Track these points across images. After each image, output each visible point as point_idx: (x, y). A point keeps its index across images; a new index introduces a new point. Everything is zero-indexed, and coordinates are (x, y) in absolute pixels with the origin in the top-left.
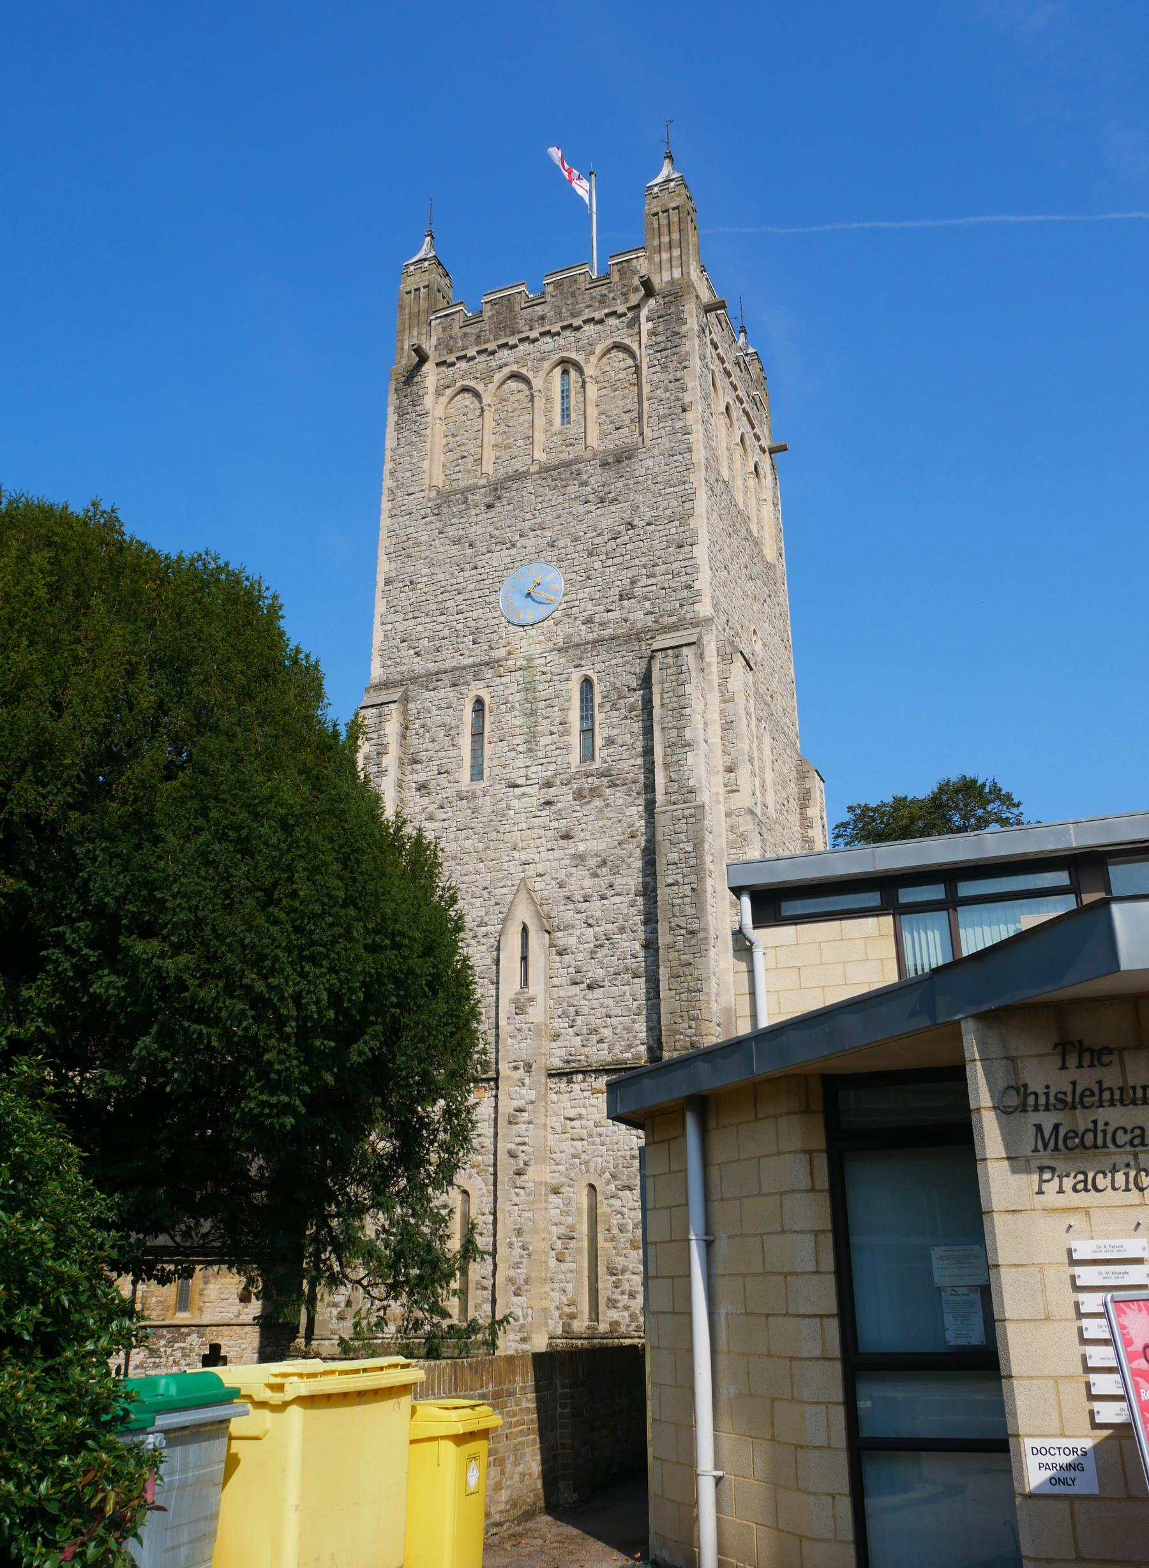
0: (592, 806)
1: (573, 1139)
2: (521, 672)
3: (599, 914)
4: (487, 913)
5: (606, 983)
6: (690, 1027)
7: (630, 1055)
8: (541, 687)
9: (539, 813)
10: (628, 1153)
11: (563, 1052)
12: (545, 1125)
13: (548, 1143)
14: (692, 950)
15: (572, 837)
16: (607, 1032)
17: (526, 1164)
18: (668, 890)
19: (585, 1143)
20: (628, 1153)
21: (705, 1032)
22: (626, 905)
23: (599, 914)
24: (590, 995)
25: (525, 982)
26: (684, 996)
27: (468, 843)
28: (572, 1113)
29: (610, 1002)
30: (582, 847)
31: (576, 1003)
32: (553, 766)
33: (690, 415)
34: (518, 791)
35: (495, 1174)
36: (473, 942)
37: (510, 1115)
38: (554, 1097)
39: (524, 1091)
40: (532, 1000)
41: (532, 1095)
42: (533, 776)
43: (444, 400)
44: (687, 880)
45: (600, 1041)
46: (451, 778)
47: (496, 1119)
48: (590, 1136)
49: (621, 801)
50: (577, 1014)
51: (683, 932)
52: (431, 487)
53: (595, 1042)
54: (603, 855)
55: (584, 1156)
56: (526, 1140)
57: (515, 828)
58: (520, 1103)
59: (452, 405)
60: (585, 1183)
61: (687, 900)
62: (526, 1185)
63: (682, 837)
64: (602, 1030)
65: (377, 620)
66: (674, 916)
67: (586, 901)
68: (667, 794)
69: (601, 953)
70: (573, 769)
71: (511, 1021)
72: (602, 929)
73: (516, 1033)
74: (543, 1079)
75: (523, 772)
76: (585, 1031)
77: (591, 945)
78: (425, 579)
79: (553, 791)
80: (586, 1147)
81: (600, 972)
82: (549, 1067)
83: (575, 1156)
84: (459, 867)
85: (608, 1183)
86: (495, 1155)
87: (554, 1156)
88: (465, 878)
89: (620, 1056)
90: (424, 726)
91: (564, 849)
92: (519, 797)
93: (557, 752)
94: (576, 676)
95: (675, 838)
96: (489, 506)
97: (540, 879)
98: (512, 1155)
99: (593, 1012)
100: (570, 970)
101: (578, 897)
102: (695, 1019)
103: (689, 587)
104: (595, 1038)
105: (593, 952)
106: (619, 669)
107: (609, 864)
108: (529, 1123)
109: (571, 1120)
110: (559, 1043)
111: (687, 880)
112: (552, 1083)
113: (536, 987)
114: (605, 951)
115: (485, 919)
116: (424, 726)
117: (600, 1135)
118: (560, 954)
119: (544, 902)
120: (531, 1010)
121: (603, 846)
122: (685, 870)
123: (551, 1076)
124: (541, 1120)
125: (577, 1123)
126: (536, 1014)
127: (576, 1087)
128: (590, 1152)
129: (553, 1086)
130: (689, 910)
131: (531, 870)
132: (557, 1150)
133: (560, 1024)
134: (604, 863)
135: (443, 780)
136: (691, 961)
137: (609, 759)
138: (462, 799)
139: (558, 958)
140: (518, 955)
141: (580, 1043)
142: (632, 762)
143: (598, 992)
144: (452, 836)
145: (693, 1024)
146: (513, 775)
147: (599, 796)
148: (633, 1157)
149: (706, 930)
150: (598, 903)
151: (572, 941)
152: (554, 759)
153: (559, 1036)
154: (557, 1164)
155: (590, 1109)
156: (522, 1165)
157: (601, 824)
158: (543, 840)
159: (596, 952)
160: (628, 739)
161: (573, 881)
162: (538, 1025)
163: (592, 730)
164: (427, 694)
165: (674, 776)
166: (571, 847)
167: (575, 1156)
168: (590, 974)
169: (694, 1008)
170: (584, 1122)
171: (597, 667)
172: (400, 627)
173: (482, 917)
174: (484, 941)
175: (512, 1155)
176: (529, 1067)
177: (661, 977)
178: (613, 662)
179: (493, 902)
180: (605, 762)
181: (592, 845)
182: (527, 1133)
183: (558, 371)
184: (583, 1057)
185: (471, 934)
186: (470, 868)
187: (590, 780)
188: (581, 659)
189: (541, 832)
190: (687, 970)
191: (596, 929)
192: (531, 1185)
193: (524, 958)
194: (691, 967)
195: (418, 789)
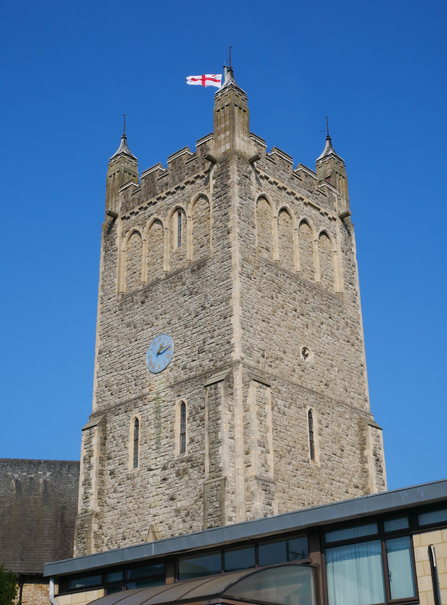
2: (154, 402)
15: (175, 499)
43: (125, 239)
52: (118, 293)
59: (129, 242)
183: (176, 214)
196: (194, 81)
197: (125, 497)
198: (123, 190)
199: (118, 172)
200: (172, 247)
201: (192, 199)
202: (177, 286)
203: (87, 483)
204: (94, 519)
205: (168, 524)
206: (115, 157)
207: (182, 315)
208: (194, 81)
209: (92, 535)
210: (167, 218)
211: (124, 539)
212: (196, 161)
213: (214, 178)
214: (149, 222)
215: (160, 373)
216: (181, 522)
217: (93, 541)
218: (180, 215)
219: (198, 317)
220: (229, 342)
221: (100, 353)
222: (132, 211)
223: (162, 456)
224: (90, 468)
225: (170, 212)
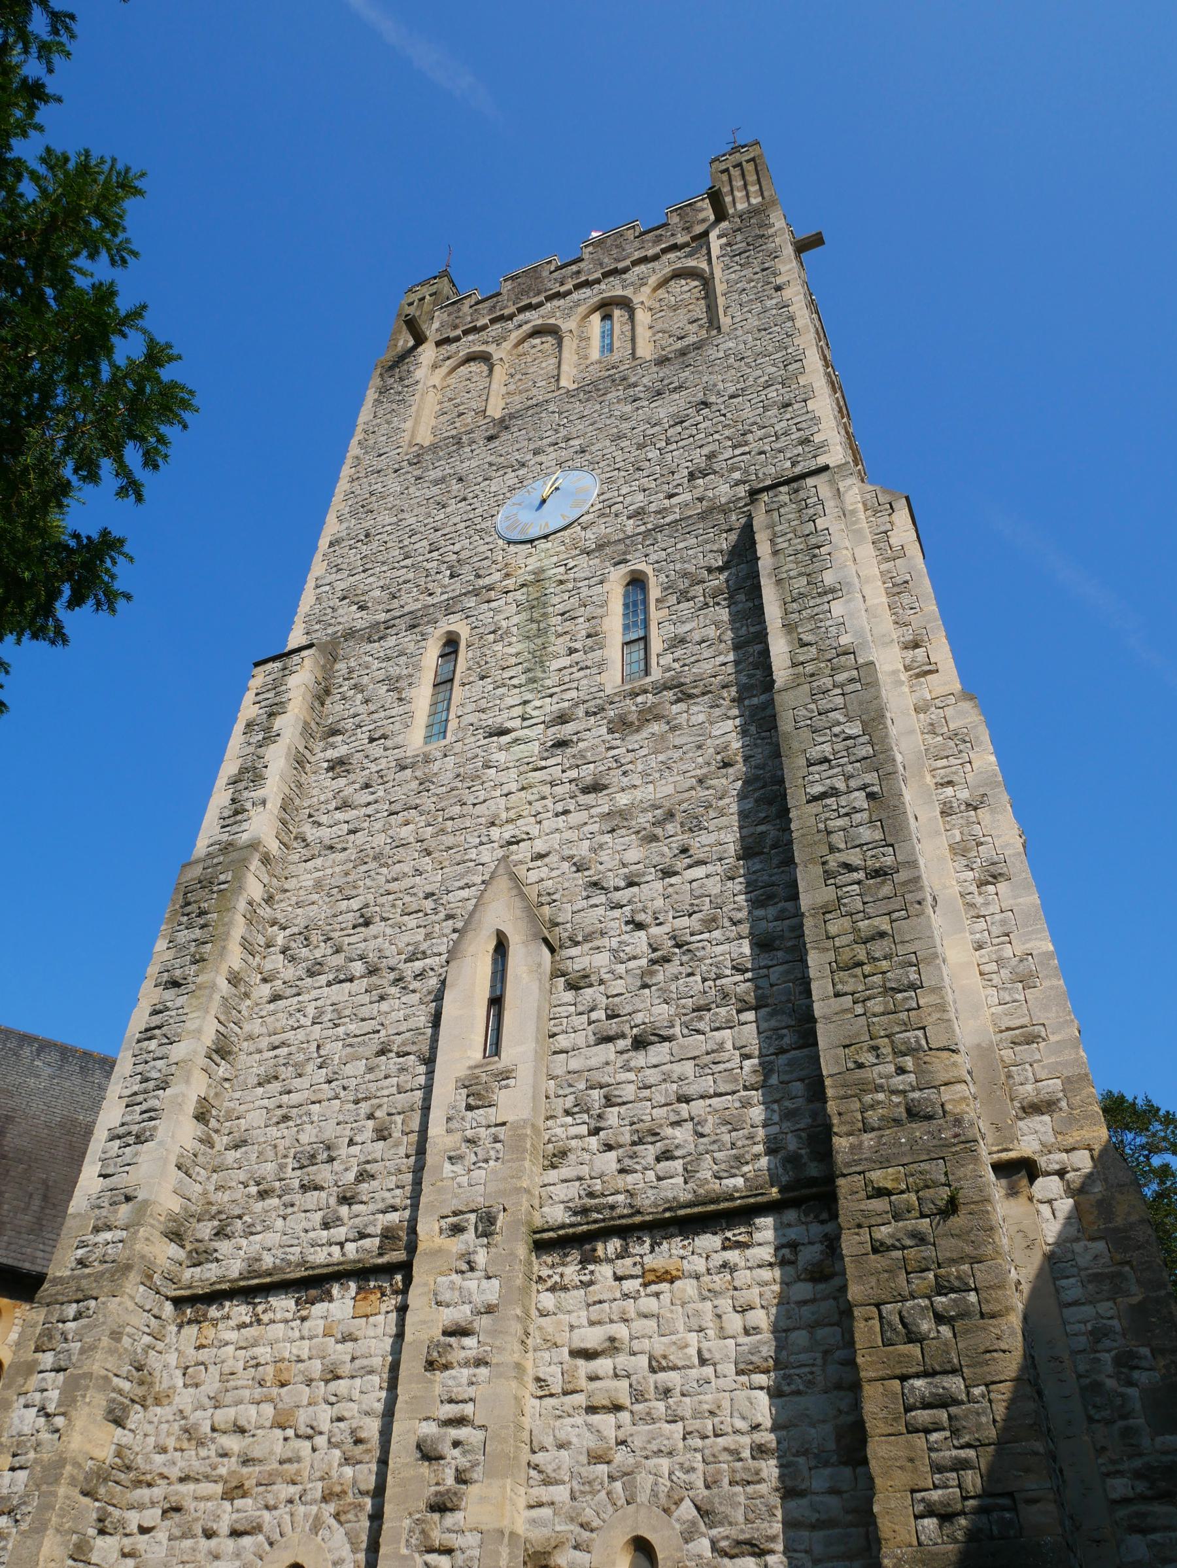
0: (645, 734)
1: (592, 1410)
2: (524, 590)
3: (659, 903)
4: (428, 936)
5: (677, 1030)
6: (901, 1071)
7: (739, 1182)
8: (556, 600)
9: (543, 763)
10: (746, 1440)
11: (573, 1191)
12: (519, 1366)
13: (526, 1422)
14: (884, 907)
15: (606, 787)
16: (682, 1135)
17: (461, 1478)
18: (815, 808)
19: (625, 1416)
20: (746, 1440)
21: (944, 1076)
22: (716, 877)
23: (659, 903)
24: (639, 1059)
25: (494, 1045)
26: (876, 1005)
27: (406, 832)
28: (592, 1338)
29: (688, 1068)
30: (623, 800)
31: (606, 1079)
32: (574, 694)
33: (787, 293)
34: (505, 739)
35: (377, 1517)
36: (393, 990)
37: (433, 1345)
38: (548, 1300)
39: (471, 1284)
40: (505, 1076)
41: (491, 1291)
42: (535, 713)
43: (444, 370)
44: (853, 783)
45: (665, 1156)
46: (389, 743)
47: (394, 1368)
48: (638, 1396)
49: (701, 718)
50: (609, 1102)
51: (860, 875)
52: (411, 445)
53: (651, 1159)
54: (667, 804)
55: (621, 1457)
56: (468, 1409)
57: (498, 793)
58: (460, 1314)
59: (453, 375)
60: (620, 1537)
61: (857, 817)
62: (456, 1541)
63: (837, 716)
64: (669, 1131)
65: (310, 583)
66: (832, 849)
67: (631, 884)
68: (794, 665)
69: (661, 975)
70: (609, 691)
71: (454, 1125)
72: (666, 928)
73: (464, 1148)
74: (522, 1250)
75: (518, 711)
76: (626, 1138)
77: (644, 962)
78: (389, 528)
79: (569, 728)
80: (628, 1428)
81: (663, 1011)
82: (538, 1222)
83: (596, 1458)
84: (384, 870)
85: (688, 1536)
86: (383, 1462)
87: (539, 1458)
88: (394, 886)
89: (715, 1185)
90: (355, 686)
91: (588, 808)
92: (507, 747)
93: (582, 673)
94: (617, 577)
95: (820, 722)
96: (490, 438)
97: (539, 863)
98: (428, 1454)
99: (646, 1093)
100: (594, 1016)
101: (611, 881)
102: (910, 1051)
103: (805, 441)
104: (649, 1152)
105: (646, 973)
106: (690, 552)
107: (679, 817)
108: (480, 1362)
109: (588, 1355)
110: (565, 1172)
111: (853, 783)
112: (542, 1266)
113: (519, 1046)
114: (673, 968)
115: (424, 946)
116: (355, 686)
117: (667, 1392)
118: (573, 986)
119: (544, 899)
120: (502, 1097)
121: (670, 790)
122: (849, 768)
123: (541, 1246)
124: (511, 1353)
125: (603, 1365)
126: (513, 1104)
127: (604, 1272)
128: (637, 1443)
129: (545, 1272)
130: (867, 834)
131: (522, 852)
132: (548, 1441)
133: (566, 1129)
134: (670, 815)
135: (376, 750)
136: (886, 927)
137: (676, 665)
138: (404, 768)
139: (569, 996)
140: (483, 993)
141: (615, 1166)
142: (721, 659)
143: (659, 1052)
144: (378, 825)
145: (908, 1062)
146: (499, 720)
147: (657, 718)
148: (760, 1451)
149: (913, 864)
150: (658, 885)
151: (602, 960)
152: (575, 685)
153: (564, 1154)
154: (547, 1482)
155: (639, 1325)
156: (450, 1481)
157: (661, 757)
158: (549, 802)
159: (652, 973)
160: (712, 632)
161: (604, 856)
162: (516, 1126)
163: (645, 639)
164: (369, 647)
165: (807, 638)
166: (602, 803)
167: (596, 1458)
168: (639, 1018)
169: (907, 1026)
170: (622, 1360)
171: (653, 557)
172: (341, 585)
173: (417, 944)
174: (415, 985)
175: (428, 1454)
176: (487, 1224)
177: (812, 973)
178: (679, 546)
179: (442, 915)
180: (669, 669)
181: (646, 793)
182: (471, 1392)
183: (596, 318)
184: (621, 1198)
185: (392, 976)
186: (406, 868)
187: (639, 699)
188: (624, 553)
189: (546, 790)
190: (879, 948)
191: (654, 930)
192: (472, 1539)
193: (496, 1002)
194: (885, 942)
195: (331, 769)
197: (386, 814)
201: (653, 281)
203: (251, 774)
204: (255, 864)
205: (572, 857)
209: (242, 905)
211: (367, 924)
215: (546, 537)
216: (635, 844)
217: (239, 928)
218: (607, 317)
221: (331, 544)
223: (551, 696)
224: (270, 737)
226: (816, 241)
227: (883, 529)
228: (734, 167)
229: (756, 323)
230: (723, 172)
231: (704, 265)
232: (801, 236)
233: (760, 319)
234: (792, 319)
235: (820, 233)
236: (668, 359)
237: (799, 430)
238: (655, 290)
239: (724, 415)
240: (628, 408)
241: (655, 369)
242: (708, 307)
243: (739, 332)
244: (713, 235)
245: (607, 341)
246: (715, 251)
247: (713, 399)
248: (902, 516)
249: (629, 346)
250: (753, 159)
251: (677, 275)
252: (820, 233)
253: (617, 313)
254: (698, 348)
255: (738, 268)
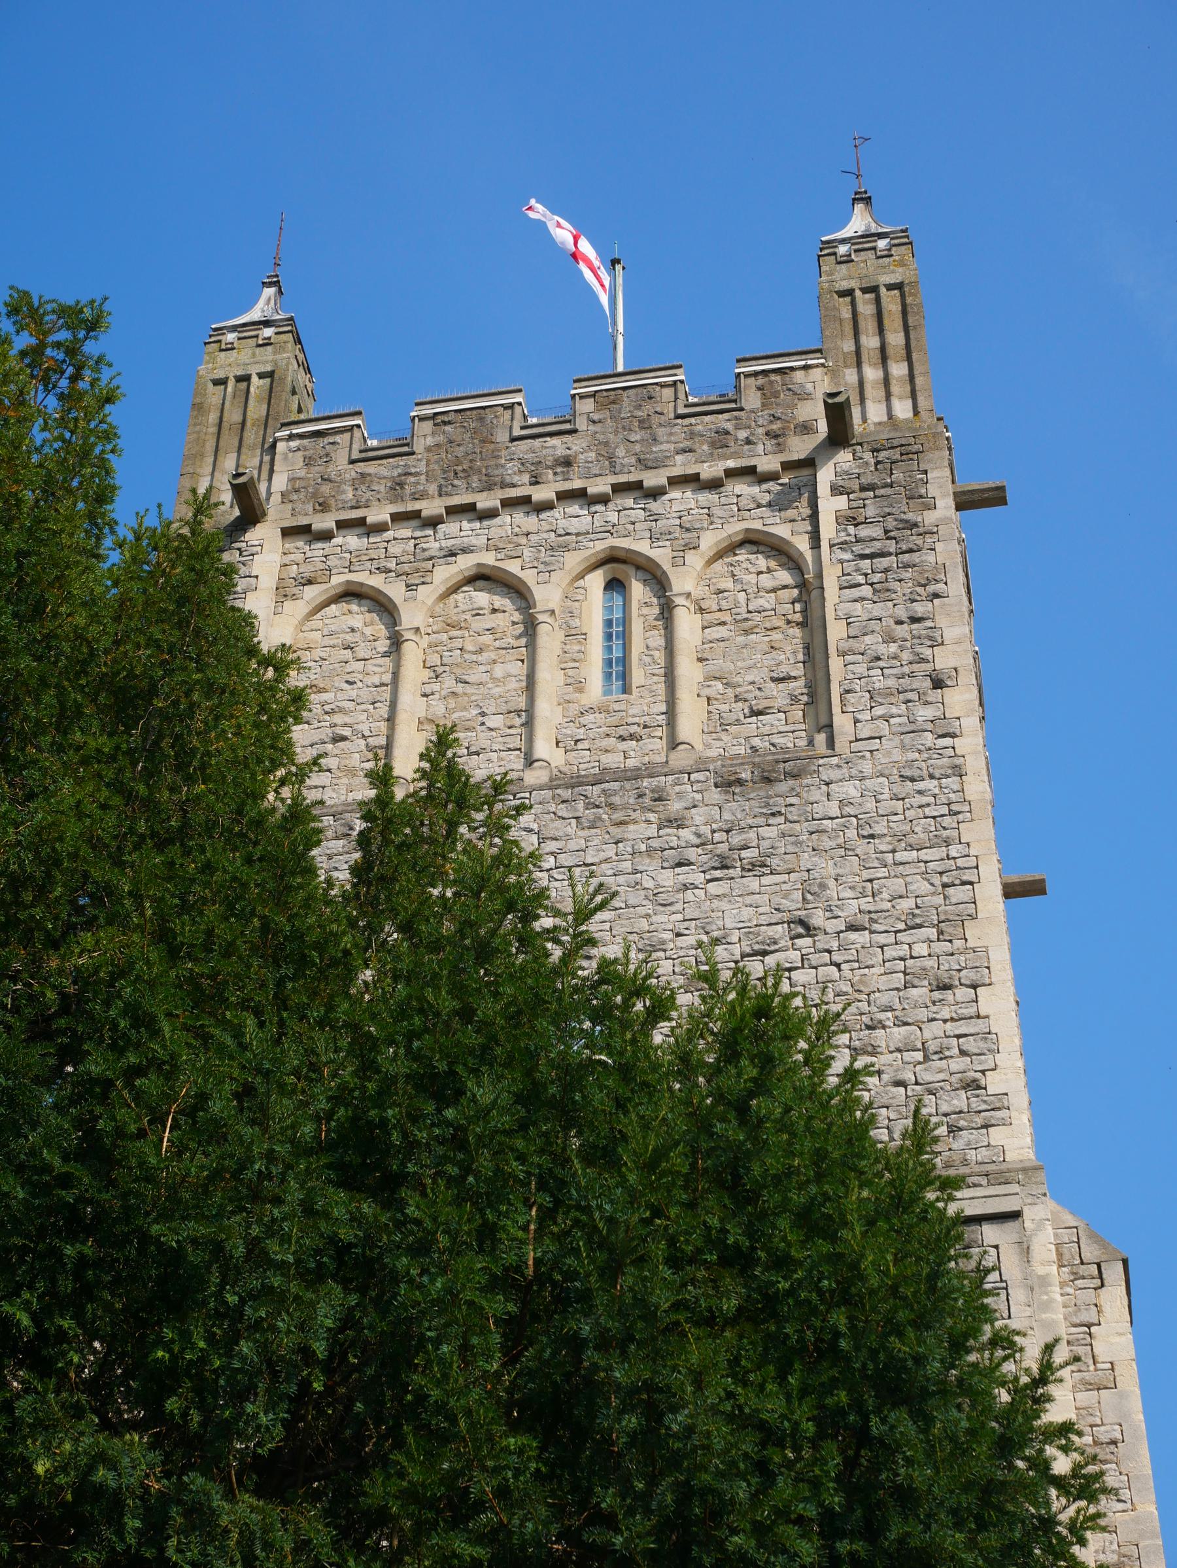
59: (315, 623)
103: (973, 1086)
183: (596, 581)
196: (538, 211)
198: (301, 436)
199: (261, 376)
200: (578, 686)
201: (709, 541)
202: (635, 822)
206: (244, 325)
207: (668, 936)
208: (538, 211)
210: (560, 579)
212: (736, 418)
213: (836, 490)
214: (444, 574)
218: (615, 585)
219: (768, 959)
220: (973, 1086)
222: (412, 506)
225: (573, 560)
226: (1035, 888)
227: (1085, 1317)
228: (865, 291)
229: (897, 755)
230: (843, 294)
231: (802, 544)
232: (1014, 878)
233: (903, 747)
234: (959, 772)
235: (1043, 881)
236: (740, 782)
237: (963, 1053)
238: (711, 562)
239: (838, 966)
240: (668, 878)
241: (715, 795)
242: (807, 648)
243: (867, 767)
244: (825, 476)
245: (617, 653)
246: (830, 506)
247: (818, 919)
248: (1114, 1297)
249: (661, 689)
250: (899, 286)
251: (753, 541)
252: (1043, 881)
253: (638, 590)
254: (794, 776)
255: (866, 591)
